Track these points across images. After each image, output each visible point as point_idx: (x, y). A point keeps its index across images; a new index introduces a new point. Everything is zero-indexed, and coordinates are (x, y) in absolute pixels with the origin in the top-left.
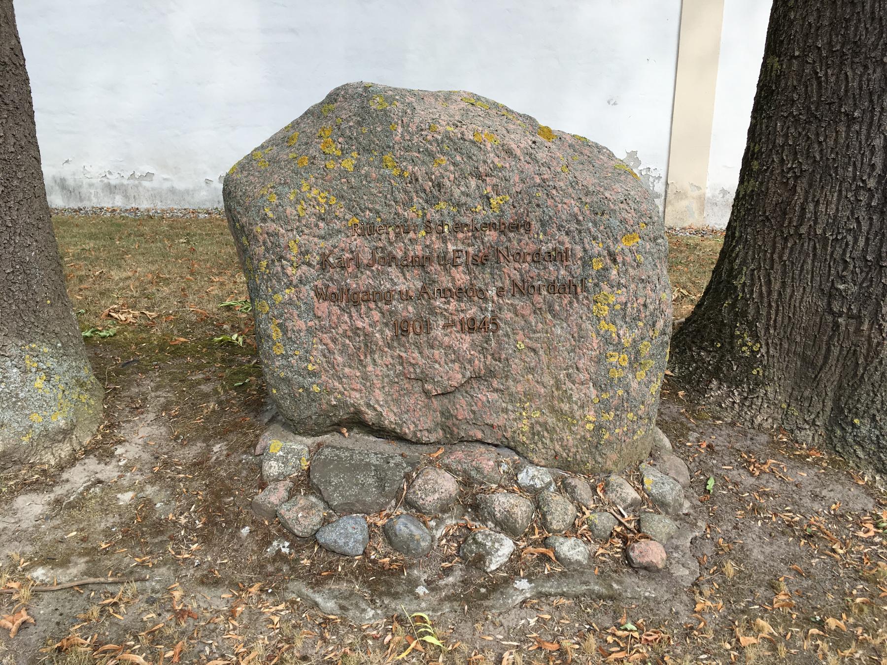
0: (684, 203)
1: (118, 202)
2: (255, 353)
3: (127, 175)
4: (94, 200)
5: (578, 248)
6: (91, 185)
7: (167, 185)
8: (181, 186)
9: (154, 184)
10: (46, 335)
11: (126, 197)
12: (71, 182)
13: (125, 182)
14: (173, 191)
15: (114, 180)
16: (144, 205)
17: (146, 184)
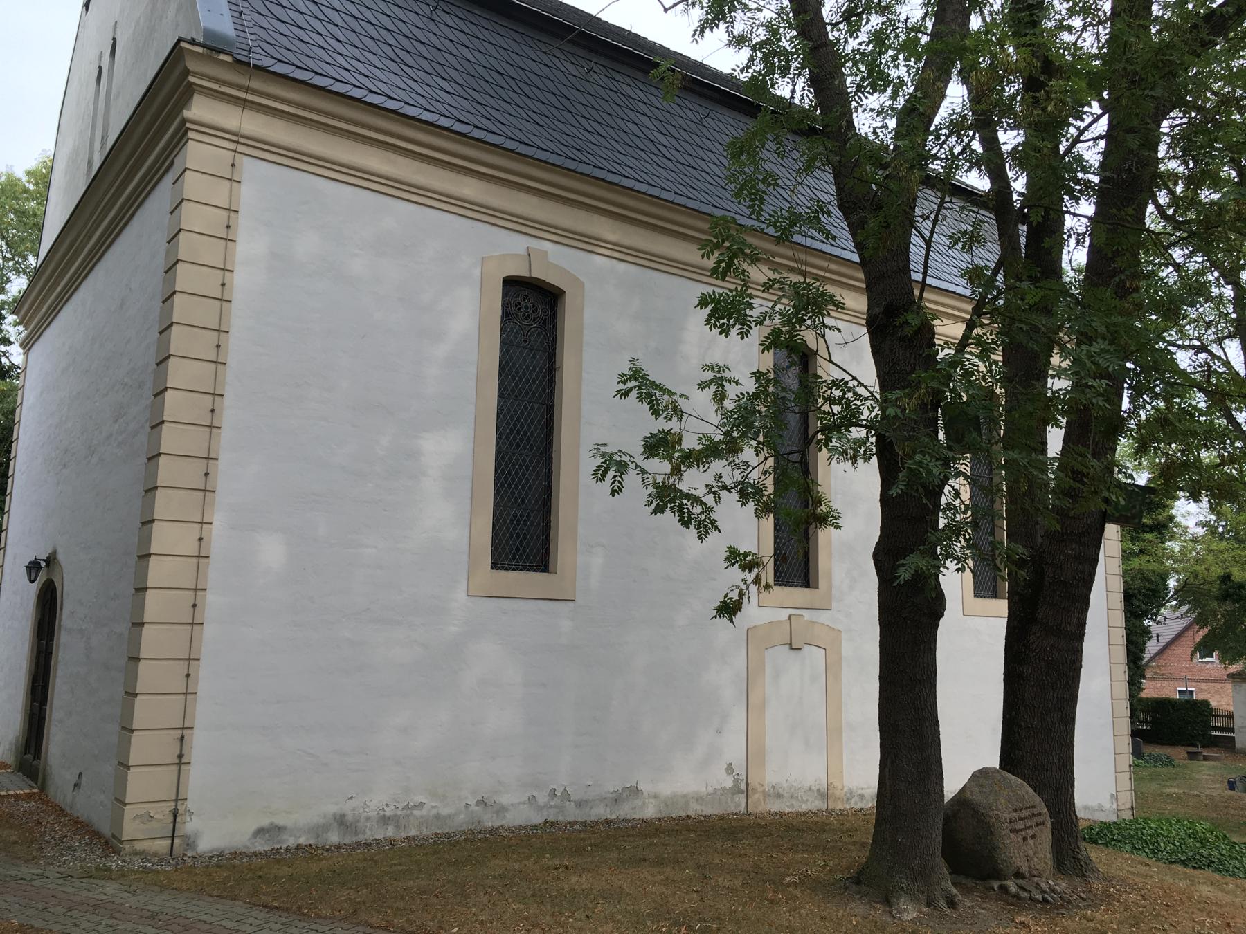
0: (756, 796)
1: (390, 832)
2: (719, 302)
3: (400, 806)
4: (368, 833)
5: (251, 882)
6: (368, 819)
7: (434, 812)
8: (445, 811)
9: (424, 812)
10: (1145, 643)
11: (397, 827)
12: (350, 818)
13: (399, 813)
14: (438, 817)
15: (389, 812)
16: (413, 832)
17: (417, 813)
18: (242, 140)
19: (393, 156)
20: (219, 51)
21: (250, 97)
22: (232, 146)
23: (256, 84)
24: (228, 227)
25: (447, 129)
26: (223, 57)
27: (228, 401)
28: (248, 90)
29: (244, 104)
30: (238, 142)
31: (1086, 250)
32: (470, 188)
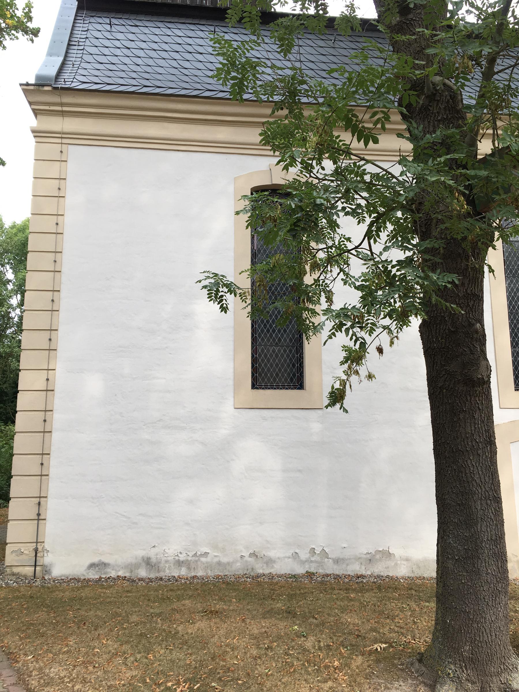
20: (43, 85)
21: (65, 109)
22: (59, 141)
23: (66, 99)
26: (46, 88)
27: (63, 294)
28: (62, 104)
29: (63, 114)
30: (62, 138)
32: (223, 134)
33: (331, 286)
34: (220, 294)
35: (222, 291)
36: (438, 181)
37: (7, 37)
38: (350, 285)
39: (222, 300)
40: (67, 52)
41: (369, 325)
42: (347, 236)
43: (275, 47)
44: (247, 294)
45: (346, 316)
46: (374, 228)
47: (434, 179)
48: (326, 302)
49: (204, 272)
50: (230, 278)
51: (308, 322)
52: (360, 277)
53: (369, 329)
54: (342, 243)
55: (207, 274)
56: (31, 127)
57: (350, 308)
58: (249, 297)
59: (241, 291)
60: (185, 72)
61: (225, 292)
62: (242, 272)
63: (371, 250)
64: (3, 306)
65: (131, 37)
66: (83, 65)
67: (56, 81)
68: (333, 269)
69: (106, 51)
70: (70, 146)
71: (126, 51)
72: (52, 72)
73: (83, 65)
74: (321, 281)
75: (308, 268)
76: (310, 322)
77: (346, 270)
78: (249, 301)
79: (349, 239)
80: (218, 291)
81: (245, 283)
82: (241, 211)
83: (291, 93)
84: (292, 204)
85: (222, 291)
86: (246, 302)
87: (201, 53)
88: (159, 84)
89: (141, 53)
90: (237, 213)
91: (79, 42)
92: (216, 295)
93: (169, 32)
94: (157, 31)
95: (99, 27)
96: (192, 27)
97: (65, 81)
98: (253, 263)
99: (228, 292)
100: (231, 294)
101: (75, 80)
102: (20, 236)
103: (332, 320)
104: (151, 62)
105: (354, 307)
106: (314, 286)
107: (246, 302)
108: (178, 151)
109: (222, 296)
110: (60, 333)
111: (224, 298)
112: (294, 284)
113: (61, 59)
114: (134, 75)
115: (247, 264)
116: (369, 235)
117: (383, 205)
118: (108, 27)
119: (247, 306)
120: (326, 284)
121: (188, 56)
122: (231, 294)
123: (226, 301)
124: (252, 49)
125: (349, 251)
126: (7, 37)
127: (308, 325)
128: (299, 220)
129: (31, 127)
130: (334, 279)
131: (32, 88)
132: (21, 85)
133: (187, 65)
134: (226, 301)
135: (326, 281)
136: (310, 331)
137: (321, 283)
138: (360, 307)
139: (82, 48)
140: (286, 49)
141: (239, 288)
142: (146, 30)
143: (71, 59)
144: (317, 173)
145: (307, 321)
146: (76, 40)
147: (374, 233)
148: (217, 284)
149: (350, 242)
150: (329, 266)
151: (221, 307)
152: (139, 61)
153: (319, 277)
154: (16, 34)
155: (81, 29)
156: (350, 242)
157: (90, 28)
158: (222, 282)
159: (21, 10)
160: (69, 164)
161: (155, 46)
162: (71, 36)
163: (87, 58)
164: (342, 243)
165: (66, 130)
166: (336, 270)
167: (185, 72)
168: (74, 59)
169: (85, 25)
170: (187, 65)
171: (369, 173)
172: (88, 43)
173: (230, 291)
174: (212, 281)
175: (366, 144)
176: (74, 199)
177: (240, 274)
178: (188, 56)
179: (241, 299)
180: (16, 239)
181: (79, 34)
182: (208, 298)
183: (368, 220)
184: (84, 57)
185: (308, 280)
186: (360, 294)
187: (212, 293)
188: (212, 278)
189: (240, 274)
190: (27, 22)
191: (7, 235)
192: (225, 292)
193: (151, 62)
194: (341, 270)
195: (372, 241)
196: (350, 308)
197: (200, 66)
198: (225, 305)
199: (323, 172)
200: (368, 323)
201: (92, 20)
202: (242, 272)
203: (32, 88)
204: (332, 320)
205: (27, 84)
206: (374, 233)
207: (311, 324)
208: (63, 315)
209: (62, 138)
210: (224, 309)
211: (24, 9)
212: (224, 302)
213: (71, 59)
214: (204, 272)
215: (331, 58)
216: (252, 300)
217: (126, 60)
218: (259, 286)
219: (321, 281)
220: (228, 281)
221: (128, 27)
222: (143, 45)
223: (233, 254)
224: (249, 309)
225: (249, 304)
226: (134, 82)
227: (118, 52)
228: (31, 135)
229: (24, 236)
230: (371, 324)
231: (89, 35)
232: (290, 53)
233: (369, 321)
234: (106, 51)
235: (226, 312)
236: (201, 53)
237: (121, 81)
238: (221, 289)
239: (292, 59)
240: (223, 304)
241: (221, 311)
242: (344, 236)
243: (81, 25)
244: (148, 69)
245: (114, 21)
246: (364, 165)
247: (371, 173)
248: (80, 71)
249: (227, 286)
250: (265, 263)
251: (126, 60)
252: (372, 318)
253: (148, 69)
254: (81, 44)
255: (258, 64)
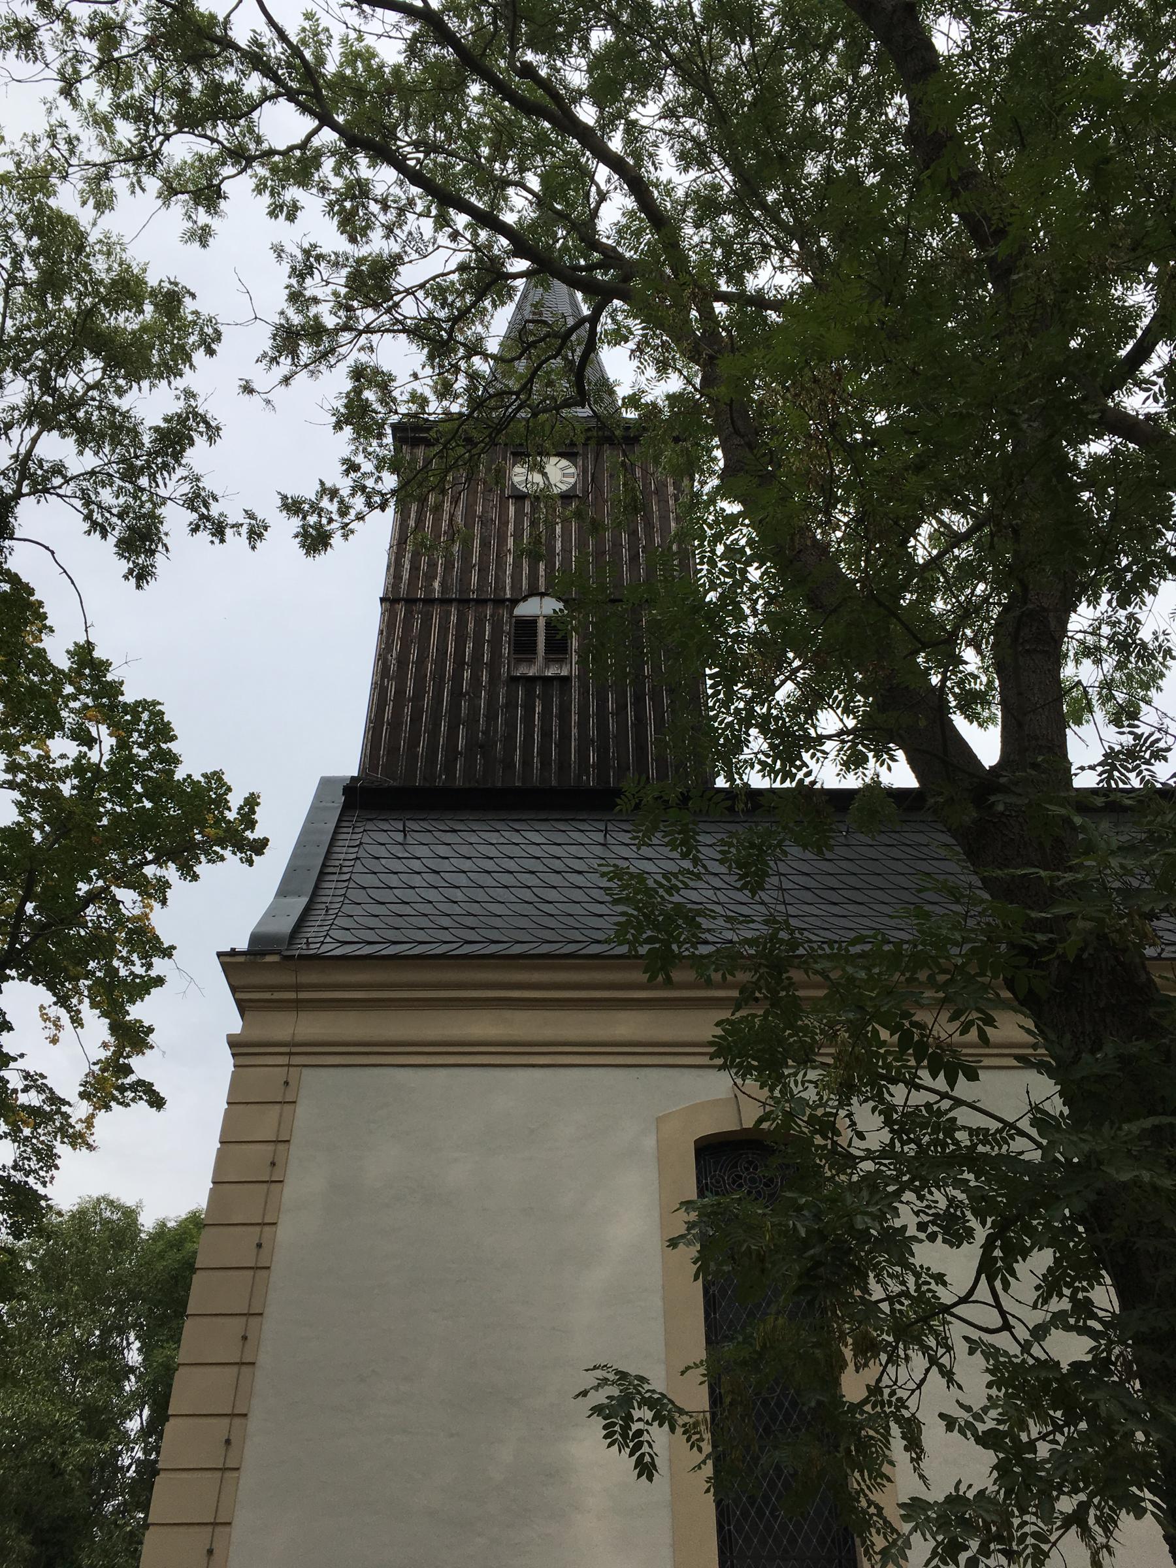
18: (294, 1050)
19: (508, 1014)
20: (263, 954)
21: (303, 995)
22: (283, 1060)
23: (307, 978)
24: (273, 1164)
25: (443, 956)
26: (269, 959)
27: (254, 1423)
28: (298, 988)
29: (298, 1006)
30: (290, 1054)
31: (999, 728)
32: (626, 1026)
33: (912, 1403)
34: (636, 1426)
35: (640, 1420)
36: (1137, 1182)
37: (202, 858)
38: (962, 1432)
39: (639, 1446)
40: (317, 887)
41: (1030, 1540)
42: (934, 1270)
43: (732, 879)
44: (703, 1428)
45: (969, 1526)
46: (998, 1253)
47: (1125, 1177)
48: (906, 1449)
49: (595, 1368)
50: (658, 1383)
51: (864, 1504)
52: (985, 1410)
53: (1029, 1550)
54: (924, 1288)
55: (600, 1373)
56: (229, 1036)
57: (970, 1495)
58: (707, 1436)
59: (686, 1419)
60: (546, 908)
61: (647, 1423)
62: (688, 1368)
63: (998, 1305)
64: (106, 1440)
65: (442, 850)
66: (347, 909)
67: (290, 944)
68: (910, 1352)
69: (393, 880)
70: (305, 1071)
71: (432, 878)
72: (285, 925)
73: (347, 909)
74: (887, 1391)
75: (848, 1353)
76: (870, 1503)
77: (945, 1360)
78: (707, 1448)
79: (940, 1279)
80: (629, 1418)
81: (694, 1397)
82: (682, 1236)
83: (773, 962)
84: (799, 1225)
85: (640, 1420)
86: (700, 1450)
87: (580, 873)
88: (494, 935)
89: (462, 880)
90: (673, 1243)
91: (341, 866)
92: (626, 1428)
93: (516, 838)
94: (494, 838)
95: (382, 837)
96: (561, 826)
97: (308, 943)
98: (711, 1340)
99: (654, 1419)
100: (661, 1425)
101: (328, 939)
102: (172, 1259)
103: (928, 1536)
104: (480, 895)
105: (982, 1493)
106: (868, 1408)
107: (700, 1450)
108: (533, 1066)
109: (639, 1433)
110: (238, 1532)
111: (646, 1437)
112: (819, 1403)
113: (303, 901)
114: (446, 922)
115: (698, 1351)
116: (987, 1268)
117: (1014, 1205)
118: (399, 837)
119: (704, 1462)
120: (900, 1399)
121: (554, 879)
122: (661, 1425)
123: (650, 1446)
124: (687, 887)
125: (947, 1309)
126: (202, 858)
127: (865, 1512)
128: (818, 1264)
129: (229, 1036)
130: (919, 1386)
131: (241, 959)
132: (219, 955)
133: (552, 895)
134: (650, 1446)
135: (901, 1393)
136: (873, 1531)
137: (886, 1397)
138: (998, 1492)
139: (347, 877)
140: (752, 874)
141: (681, 1412)
142: (473, 839)
143: (324, 899)
144: (849, 1145)
145: (862, 1499)
146: (337, 863)
147: (1000, 1263)
148: (625, 1402)
149: (945, 1284)
150: (901, 1345)
151: (639, 1463)
152: (458, 895)
153: (879, 1380)
154: (221, 852)
155: (347, 843)
156: (945, 1284)
157: (366, 840)
158: (639, 1393)
159: (235, 810)
160: (301, 1110)
161: (489, 865)
162: (326, 858)
163: (354, 895)
164: (924, 1288)
165: (299, 1038)
166: (919, 1361)
167: (546, 908)
168: (329, 899)
169: (355, 836)
170: (552, 895)
171: (964, 1128)
172: (359, 867)
173: (660, 1418)
174: (615, 1391)
175: (952, 1083)
176: (304, 1183)
177: (683, 1373)
178: (554, 879)
179: (688, 1440)
180: (160, 1266)
181: (343, 853)
182: (605, 1437)
183: (981, 1234)
184: (350, 893)
185: (853, 1386)
186: (990, 1457)
187: (614, 1424)
188: (613, 1383)
189: (683, 1373)
190: (244, 830)
191: (142, 1257)
192: (647, 1423)
193: (480, 895)
194: (933, 1361)
195: (998, 1284)
196: (970, 1495)
197: (577, 895)
198: (647, 1459)
199: (863, 1145)
200: (1025, 1535)
201: (370, 826)
202: (688, 1368)
203: (241, 959)
204: (928, 1536)
205: (233, 953)
206: (1000, 1263)
207: (872, 1510)
208: (248, 1480)
209: (290, 1054)
210: (646, 1469)
211: (241, 808)
212: (645, 1448)
213: (324, 899)
214: (595, 1368)
215: (844, 864)
216: (714, 1447)
217: (432, 895)
218: (731, 1404)
219: (887, 1391)
220: (653, 1391)
221: (436, 834)
222: (466, 865)
223: (660, 1304)
224: (708, 1470)
225: (708, 1457)
226: (447, 936)
227: (416, 880)
228: (228, 1051)
229: (179, 1257)
230: (1034, 1535)
231: (362, 854)
232: (763, 889)
233: (1027, 1529)
234: (393, 880)
235: (650, 1478)
236: (580, 873)
237: (421, 936)
238: (636, 1414)
239: (767, 899)
240: (643, 1455)
241: (639, 1476)
242: (928, 1269)
243: (348, 837)
244: (475, 908)
245: (411, 825)
246: (951, 1109)
247: (970, 1129)
248: (340, 922)
249: (650, 1403)
250: (740, 1339)
251: (432, 895)
252: (1034, 1519)
253: (475, 908)
254: (345, 870)
255: (700, 913)
